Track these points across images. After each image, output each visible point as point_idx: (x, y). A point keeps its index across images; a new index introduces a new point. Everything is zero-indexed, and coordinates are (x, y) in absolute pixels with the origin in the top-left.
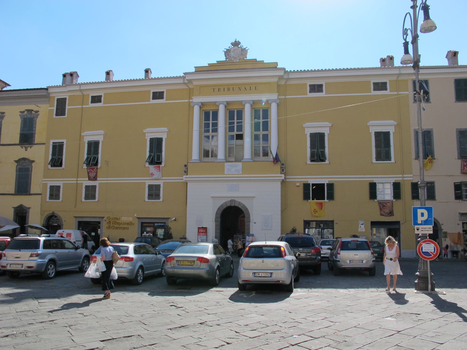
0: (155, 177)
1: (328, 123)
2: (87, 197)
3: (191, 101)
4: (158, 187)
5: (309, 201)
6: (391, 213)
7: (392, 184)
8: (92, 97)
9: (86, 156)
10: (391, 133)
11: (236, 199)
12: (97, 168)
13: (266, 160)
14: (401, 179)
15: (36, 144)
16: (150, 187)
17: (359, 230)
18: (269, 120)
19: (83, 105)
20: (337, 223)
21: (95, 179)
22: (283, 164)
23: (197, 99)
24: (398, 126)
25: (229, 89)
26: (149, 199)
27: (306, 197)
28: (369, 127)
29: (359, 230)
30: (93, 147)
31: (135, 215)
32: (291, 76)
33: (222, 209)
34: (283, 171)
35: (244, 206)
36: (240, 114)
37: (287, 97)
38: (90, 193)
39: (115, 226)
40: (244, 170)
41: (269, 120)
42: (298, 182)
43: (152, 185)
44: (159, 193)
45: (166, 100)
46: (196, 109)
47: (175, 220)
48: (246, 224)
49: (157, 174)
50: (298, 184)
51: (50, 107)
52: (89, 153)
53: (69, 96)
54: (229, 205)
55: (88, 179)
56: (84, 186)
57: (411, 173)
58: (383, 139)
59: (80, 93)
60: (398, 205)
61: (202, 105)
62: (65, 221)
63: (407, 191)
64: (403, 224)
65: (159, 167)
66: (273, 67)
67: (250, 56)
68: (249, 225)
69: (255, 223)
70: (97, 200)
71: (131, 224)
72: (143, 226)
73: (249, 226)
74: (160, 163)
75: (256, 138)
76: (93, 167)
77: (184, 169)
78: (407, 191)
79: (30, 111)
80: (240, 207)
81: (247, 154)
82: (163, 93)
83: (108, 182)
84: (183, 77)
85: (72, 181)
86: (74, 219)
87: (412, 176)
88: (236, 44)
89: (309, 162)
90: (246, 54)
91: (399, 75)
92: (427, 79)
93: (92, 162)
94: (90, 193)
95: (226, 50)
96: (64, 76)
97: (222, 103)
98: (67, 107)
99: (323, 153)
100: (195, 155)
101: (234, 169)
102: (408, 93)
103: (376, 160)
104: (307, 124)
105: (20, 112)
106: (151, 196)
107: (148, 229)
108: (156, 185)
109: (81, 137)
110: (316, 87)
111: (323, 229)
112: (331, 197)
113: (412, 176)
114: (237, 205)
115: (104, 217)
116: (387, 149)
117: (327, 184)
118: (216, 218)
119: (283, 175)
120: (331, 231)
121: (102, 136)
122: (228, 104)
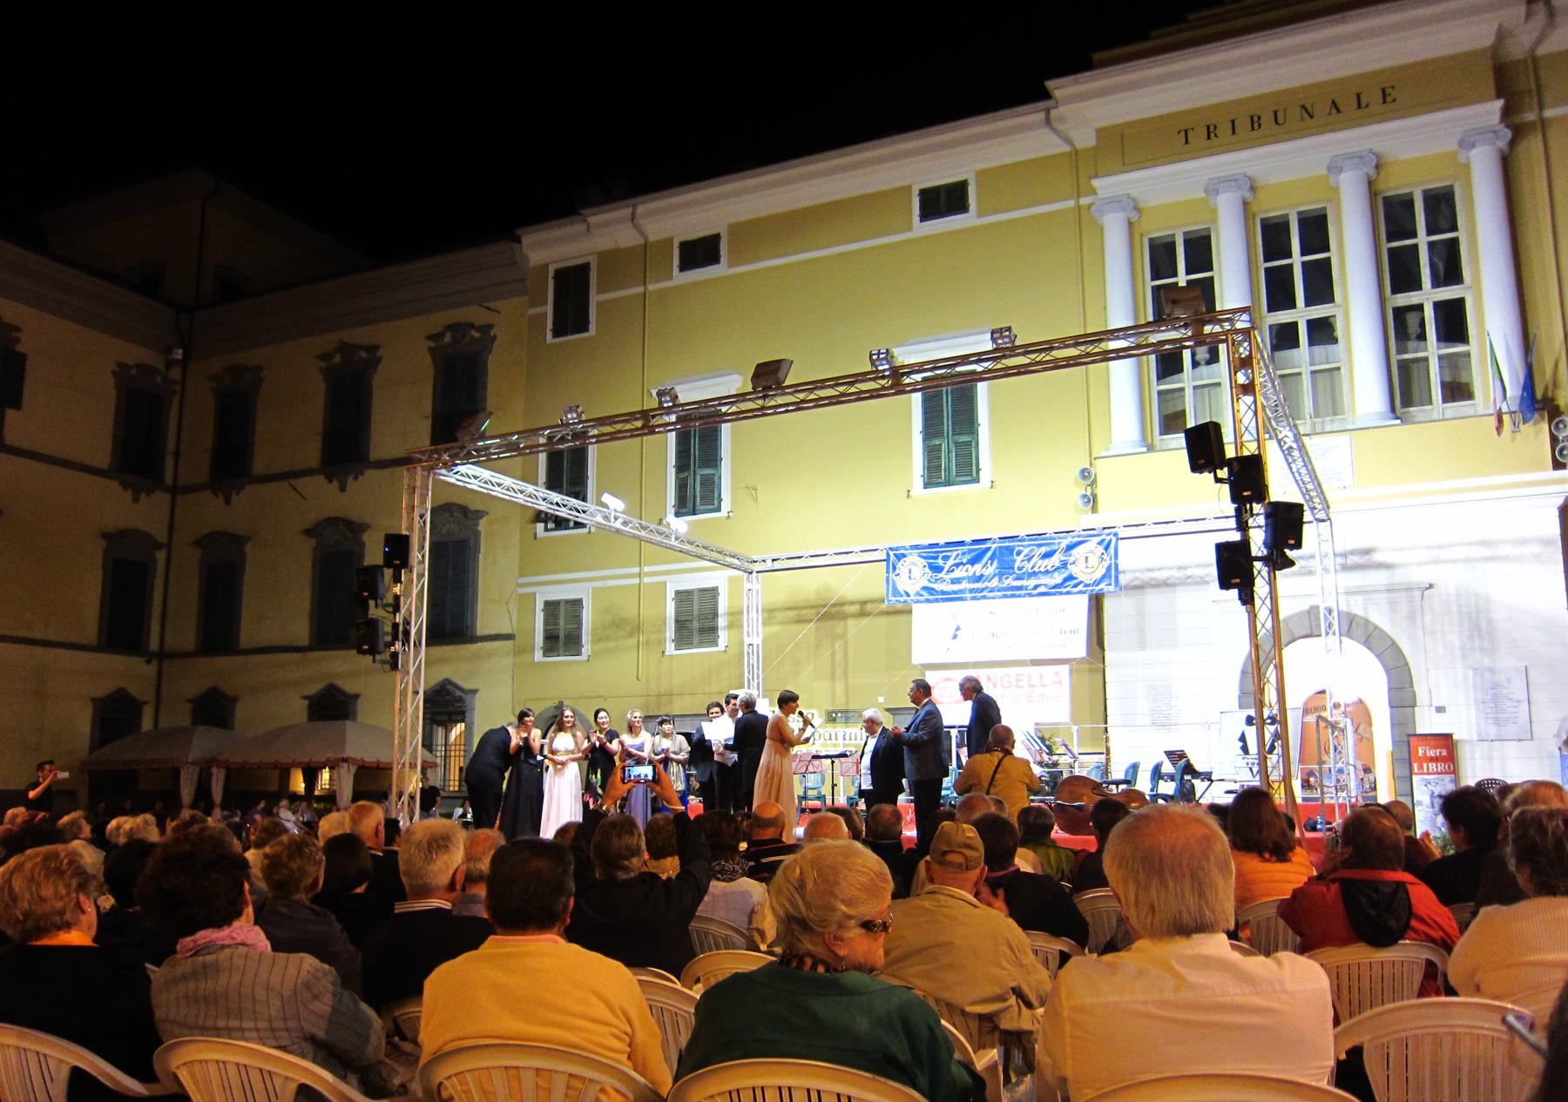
3: (1084, 201)
15: (382, 464)
18: (1385, 246)
25: (1210, 132)
41: (1385, 246)
51: (531, 306)
69: (1440, 710)
79: (458, 328)
98: (549, 309)
105: (430, 337)
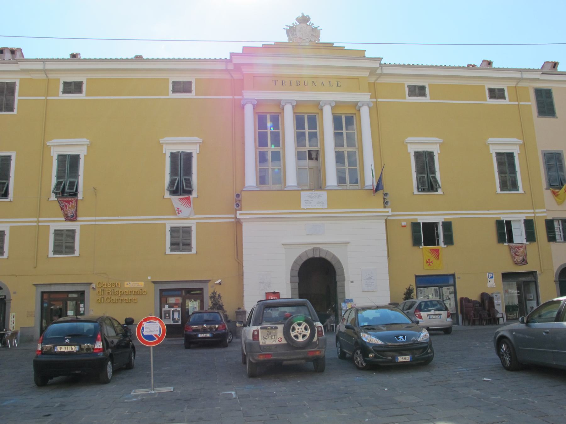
0: (187, 215)
1: (197, 138)
2: (58, 250)
4: (187, 230)
5: (421, 247)
6: (524, 262)
7: (523, 221)
8: (65, 83)
9: (54, 181)
10: (12, 158)
11: (321, 247)
12: (77, 201)
13: (274, 189)
14: (533, 215)
16: (174, 231)
17: (489, 286)
19: (47, 96)
20: (459, 278)
21: (73, 218)
22: (386, 194)
23: (250, 95)
24: (523, 146)
26: (171, 251)
27: (416, 242)
28: (488, 146)
29: (489, 286)
30: (69, 165)
31: (149, 278)
32: (386, 71)
33: (301, 263)
34: (386, 204)
35: (334, 257)
36: (277, 119)
37: (231, 97)
38: (64, 242)
39: (113, 298)
40: (331, 203)
42: (404, 220)
43: (178, 228)
44: (190, 240)
45: (196, 95)
46: (249, 111)
47: (220, 284)
48: (339, 284)
49: (186, 211)
50: (403, 224)
52: (58, 177)
53: (21, 79)
54: (311, 256)
55: (63, 219)
56: (52, 231)
57: (544, 208)
58: (506, 162)
59: (42, 76)
60: (532, 248)
61: (257, 104)
62: (15, 293)
63: (541, 231)
64: (540, 275)
65: (188, 199)
66: (360, 55)
67: (323, 39)
68: (344, 286)
69: (352, 282)
70: (77, 254)
71: (138, 292)
72: (164, 294)
73: (343, 286)
74: (190, 192)
75: (277, 156)
76: (69, 199)
77: (388, 198)
78: (541, 231)
80: (328, 258)
81: (331, 179)
82: (189, 83)
83: (97, 223)
84: (230, 61)
85: (30, 222)
86: (34, 288)
87: (545, 210)
88: (304, 20)
89: (416, 192)
90: (318, 36)
91: (520, 80)
92: (550, 88)
93: (67, 191)
94: (64, 242)
95: (288, 28)
96: (484, 61)
97: (289, 102)
98: (17, 98)
99: (189, 183)
100: (251, 180)
101: (314, 200)
102: (529, 103)
103: (501, 190)
104: (409, 138)
106: (175, 246)
107: (172, 300)
108: (68, 231)
109: (45, 149)
110: (417, 90)
111: (441, 287)
112: (449, 241)
113: (545, 210)
114: (323, 256)
115: (91, 284)
116: (512, 175)
117: (442, 222)
118: (292, 276)
119: (238, 216)
120: (452, 288)
121: (86, 147)
122: (297, 105)
